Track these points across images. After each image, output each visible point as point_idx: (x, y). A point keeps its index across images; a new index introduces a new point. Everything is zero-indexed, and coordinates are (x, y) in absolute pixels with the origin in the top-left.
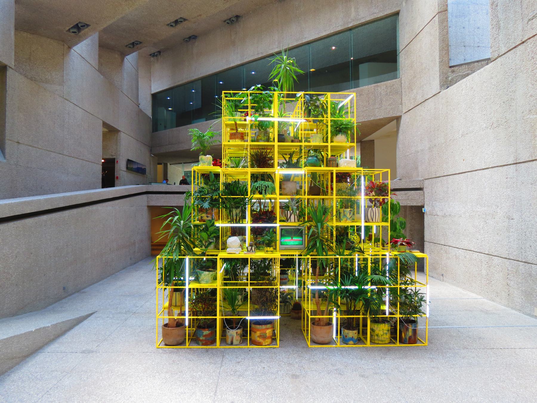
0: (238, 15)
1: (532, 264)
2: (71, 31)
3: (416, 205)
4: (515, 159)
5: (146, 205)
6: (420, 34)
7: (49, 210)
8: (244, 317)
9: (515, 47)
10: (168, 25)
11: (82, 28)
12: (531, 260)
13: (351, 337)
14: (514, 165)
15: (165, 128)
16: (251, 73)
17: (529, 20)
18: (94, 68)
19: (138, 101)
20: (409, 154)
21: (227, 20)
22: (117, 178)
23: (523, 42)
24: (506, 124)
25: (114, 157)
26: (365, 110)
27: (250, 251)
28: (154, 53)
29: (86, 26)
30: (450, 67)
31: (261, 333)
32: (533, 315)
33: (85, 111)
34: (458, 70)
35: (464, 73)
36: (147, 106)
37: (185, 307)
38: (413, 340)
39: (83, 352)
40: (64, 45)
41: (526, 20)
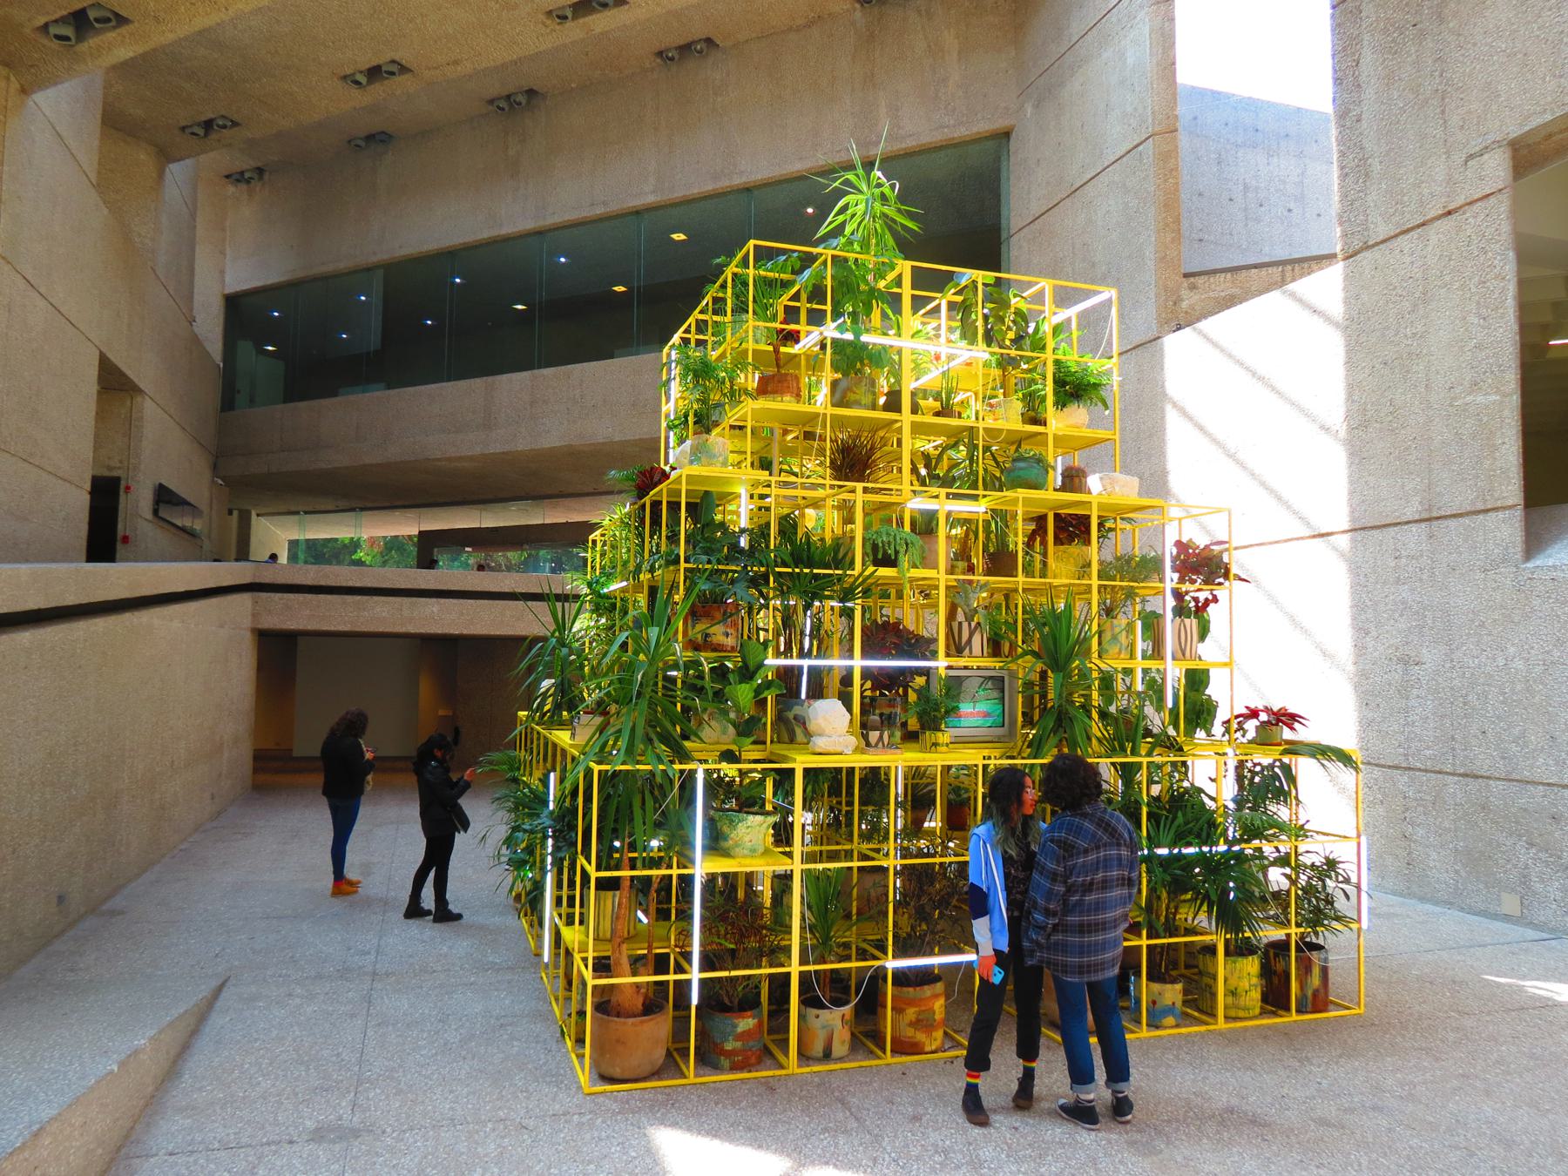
0: (535, 88)
2: (53, 30)
4: (1427, 507)
5: (249, 625)
6: (1086, 187)
7: (39, 611)
8: (876, 963)
9: (1423, 224)
10: (345, 78)
11: (97, 25)
12: (1486, 767)
13: (1170, 1003)
14: (1423, 525)
15: (252, 401)
16: (556, 259)
17: (1471, 157)
18: (87, 176)
19: (191, 310)
21: (499, 99)
22: (125, 539)
23: (1449, 213)
25: (115, 474)
27: (876, 745)
28: (242, 173)
29: (113, 23)
30: (1186, 276)
31: (919, 1013)
32: (1496, 915)
33: (55, 308)
34: (1207, 285)
35: (1223, 294)
36: (210, 326)
37: (692, 939)
38: (1318, 1002)
39: (318, 1135)
40: (8, 79)
41: (1459, 158)
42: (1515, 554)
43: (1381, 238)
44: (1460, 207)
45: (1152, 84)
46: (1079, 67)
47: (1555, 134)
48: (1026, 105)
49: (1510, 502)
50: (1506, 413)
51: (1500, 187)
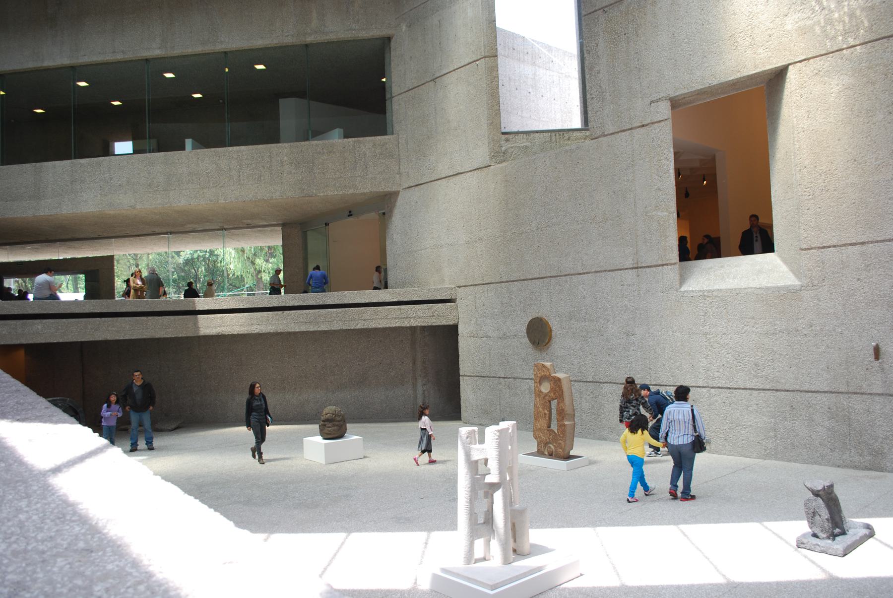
1: (666, 385)
3: (446, 324)
12: (665, 381)
14: (634, 270)
17: (652, 102)
20: (420, 249)
23: (643, 126)
24: (618, 219)
26: (339, 178)
30: (504, 133)
35: (522, 145)
41: (648, 101)
42: (676, 285)
43: (611, 132)
44: (648, 124)
45: (483, 30)
46: (438, 11)
47: (686, 97)
48: (402, 24)
49: (673, 262)
50: (671, 221)
51: (666, 118)
